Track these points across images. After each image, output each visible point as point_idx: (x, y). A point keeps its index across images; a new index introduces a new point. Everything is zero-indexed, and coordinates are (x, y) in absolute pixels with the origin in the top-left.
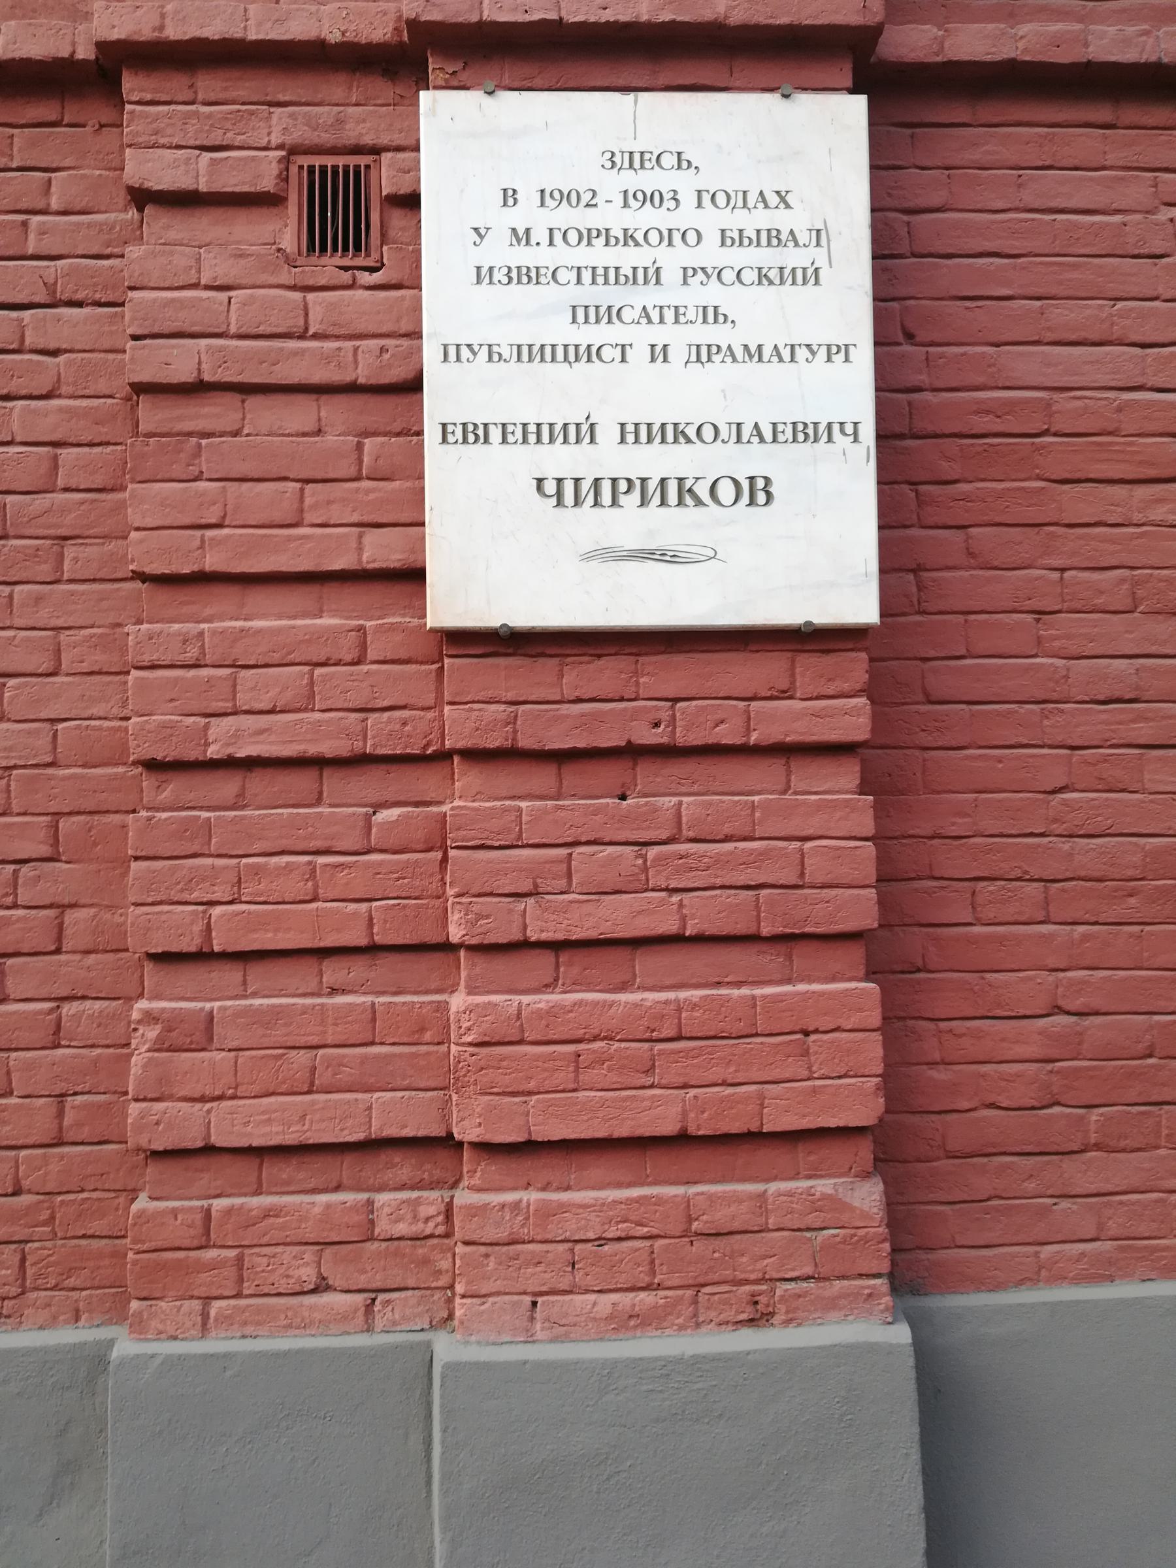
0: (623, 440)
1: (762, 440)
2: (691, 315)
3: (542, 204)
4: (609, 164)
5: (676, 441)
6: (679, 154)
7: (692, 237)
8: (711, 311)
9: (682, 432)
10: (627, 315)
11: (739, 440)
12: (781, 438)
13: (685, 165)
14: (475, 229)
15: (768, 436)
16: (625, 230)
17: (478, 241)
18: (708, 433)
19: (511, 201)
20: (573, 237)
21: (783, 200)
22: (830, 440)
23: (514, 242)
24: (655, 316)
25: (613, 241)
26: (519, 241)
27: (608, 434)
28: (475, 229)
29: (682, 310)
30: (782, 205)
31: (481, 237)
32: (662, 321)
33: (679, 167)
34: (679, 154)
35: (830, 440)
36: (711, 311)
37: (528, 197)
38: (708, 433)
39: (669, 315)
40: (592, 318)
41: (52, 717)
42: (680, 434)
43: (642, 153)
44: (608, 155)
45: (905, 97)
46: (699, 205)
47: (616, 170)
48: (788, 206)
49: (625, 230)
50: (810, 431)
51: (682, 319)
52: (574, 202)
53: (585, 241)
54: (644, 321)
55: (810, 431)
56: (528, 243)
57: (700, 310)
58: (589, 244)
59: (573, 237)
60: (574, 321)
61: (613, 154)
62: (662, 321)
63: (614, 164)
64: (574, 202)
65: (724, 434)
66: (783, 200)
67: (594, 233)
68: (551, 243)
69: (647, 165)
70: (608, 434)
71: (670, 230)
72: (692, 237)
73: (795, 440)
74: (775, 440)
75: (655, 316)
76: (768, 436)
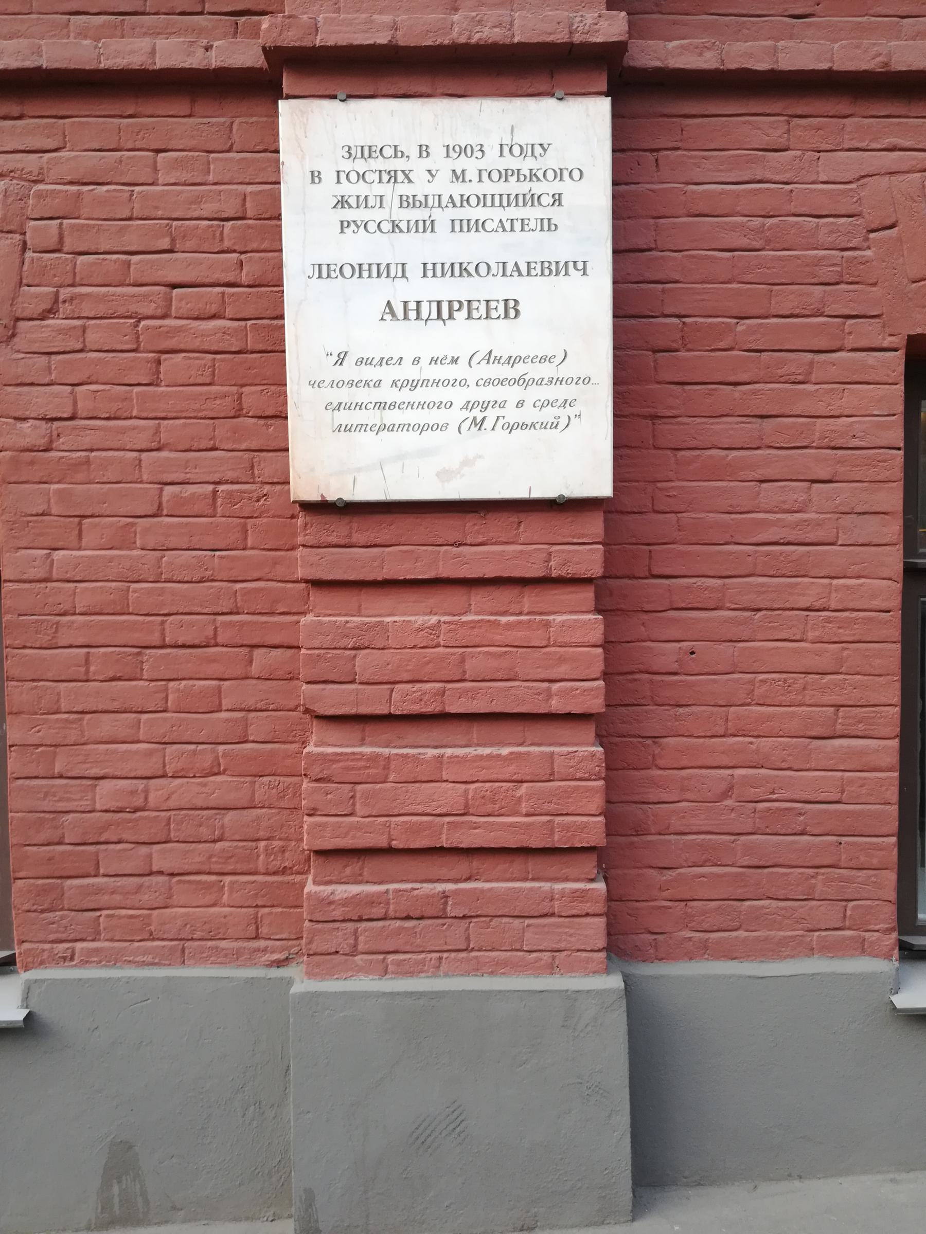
0: (425, 276)
1: (520, 274)
2: (532, 225)
3: (448, 156)
4: (347, 155)
5: (461, 275)
6: (395, 146)
7: (576, 174)
8: (546, 223)
9: (465, 269)
10: (489, 226)
11: (504, 275)
12: (533, 272)
13: (399, 154)
14: (429, 171)
15: (524, 272)
16: (531, 170)
17: (431, 180)
18: (483, 269)
19: (424, 154)
20: (495, 176)
21: (407, 177)
22: (566, 274)
23: (454, 180)
24: (508, 226)
25: (522, 178)
26: (457, 178)
27: (415, 271)
28: (429, 171)
29: (526, 222)
30: (406, 181)
31: (433, 176)
32: (512, 230)
33: (396, 156)
34: (395, 146)
35: (566, 274)
36: (546, 223)
37: (438, 151)
38: (483, 269)
39: (517, 225)
40: (465, 229)
41: (550, 678)
42: (464, 271)
43: (370, 147)
44: (346, 149)
45: (636, 90)
46: (338, 182)
47: (352, 158)
48: (410, 181)
49: (531, 170)
50: (553, 267)
51: (526, 228)
52: (469, 153)
53: (503, 179)
54: (500, 229)
55: (553, 267)
56: (463, 181)
57: (539, 221)
58: (506, 180)
59: (495, 176)
60: (453, 230)
61: (350, 148)
62: (512, 230)
63: (350, 154)
64: (469, 153)
65: (494, 270)
66: (407, 177)
67: (510, 173)
68: (480, 181)
69: (374, 155)
70: (415, 271)
71: (561, 169)
72: (576, 174)
73: (542, 274)
74: (529, 274)
75: (508, 226)
76: (524, 272)
